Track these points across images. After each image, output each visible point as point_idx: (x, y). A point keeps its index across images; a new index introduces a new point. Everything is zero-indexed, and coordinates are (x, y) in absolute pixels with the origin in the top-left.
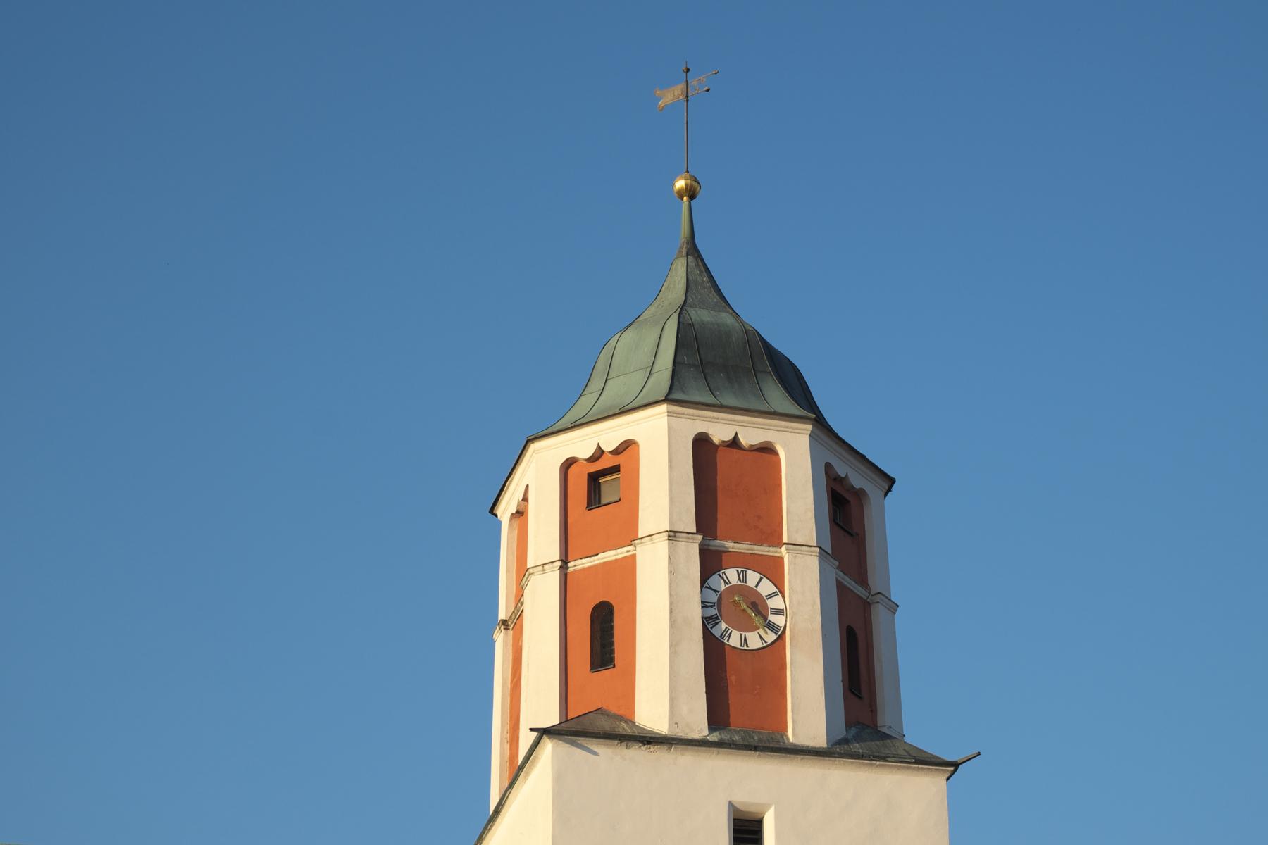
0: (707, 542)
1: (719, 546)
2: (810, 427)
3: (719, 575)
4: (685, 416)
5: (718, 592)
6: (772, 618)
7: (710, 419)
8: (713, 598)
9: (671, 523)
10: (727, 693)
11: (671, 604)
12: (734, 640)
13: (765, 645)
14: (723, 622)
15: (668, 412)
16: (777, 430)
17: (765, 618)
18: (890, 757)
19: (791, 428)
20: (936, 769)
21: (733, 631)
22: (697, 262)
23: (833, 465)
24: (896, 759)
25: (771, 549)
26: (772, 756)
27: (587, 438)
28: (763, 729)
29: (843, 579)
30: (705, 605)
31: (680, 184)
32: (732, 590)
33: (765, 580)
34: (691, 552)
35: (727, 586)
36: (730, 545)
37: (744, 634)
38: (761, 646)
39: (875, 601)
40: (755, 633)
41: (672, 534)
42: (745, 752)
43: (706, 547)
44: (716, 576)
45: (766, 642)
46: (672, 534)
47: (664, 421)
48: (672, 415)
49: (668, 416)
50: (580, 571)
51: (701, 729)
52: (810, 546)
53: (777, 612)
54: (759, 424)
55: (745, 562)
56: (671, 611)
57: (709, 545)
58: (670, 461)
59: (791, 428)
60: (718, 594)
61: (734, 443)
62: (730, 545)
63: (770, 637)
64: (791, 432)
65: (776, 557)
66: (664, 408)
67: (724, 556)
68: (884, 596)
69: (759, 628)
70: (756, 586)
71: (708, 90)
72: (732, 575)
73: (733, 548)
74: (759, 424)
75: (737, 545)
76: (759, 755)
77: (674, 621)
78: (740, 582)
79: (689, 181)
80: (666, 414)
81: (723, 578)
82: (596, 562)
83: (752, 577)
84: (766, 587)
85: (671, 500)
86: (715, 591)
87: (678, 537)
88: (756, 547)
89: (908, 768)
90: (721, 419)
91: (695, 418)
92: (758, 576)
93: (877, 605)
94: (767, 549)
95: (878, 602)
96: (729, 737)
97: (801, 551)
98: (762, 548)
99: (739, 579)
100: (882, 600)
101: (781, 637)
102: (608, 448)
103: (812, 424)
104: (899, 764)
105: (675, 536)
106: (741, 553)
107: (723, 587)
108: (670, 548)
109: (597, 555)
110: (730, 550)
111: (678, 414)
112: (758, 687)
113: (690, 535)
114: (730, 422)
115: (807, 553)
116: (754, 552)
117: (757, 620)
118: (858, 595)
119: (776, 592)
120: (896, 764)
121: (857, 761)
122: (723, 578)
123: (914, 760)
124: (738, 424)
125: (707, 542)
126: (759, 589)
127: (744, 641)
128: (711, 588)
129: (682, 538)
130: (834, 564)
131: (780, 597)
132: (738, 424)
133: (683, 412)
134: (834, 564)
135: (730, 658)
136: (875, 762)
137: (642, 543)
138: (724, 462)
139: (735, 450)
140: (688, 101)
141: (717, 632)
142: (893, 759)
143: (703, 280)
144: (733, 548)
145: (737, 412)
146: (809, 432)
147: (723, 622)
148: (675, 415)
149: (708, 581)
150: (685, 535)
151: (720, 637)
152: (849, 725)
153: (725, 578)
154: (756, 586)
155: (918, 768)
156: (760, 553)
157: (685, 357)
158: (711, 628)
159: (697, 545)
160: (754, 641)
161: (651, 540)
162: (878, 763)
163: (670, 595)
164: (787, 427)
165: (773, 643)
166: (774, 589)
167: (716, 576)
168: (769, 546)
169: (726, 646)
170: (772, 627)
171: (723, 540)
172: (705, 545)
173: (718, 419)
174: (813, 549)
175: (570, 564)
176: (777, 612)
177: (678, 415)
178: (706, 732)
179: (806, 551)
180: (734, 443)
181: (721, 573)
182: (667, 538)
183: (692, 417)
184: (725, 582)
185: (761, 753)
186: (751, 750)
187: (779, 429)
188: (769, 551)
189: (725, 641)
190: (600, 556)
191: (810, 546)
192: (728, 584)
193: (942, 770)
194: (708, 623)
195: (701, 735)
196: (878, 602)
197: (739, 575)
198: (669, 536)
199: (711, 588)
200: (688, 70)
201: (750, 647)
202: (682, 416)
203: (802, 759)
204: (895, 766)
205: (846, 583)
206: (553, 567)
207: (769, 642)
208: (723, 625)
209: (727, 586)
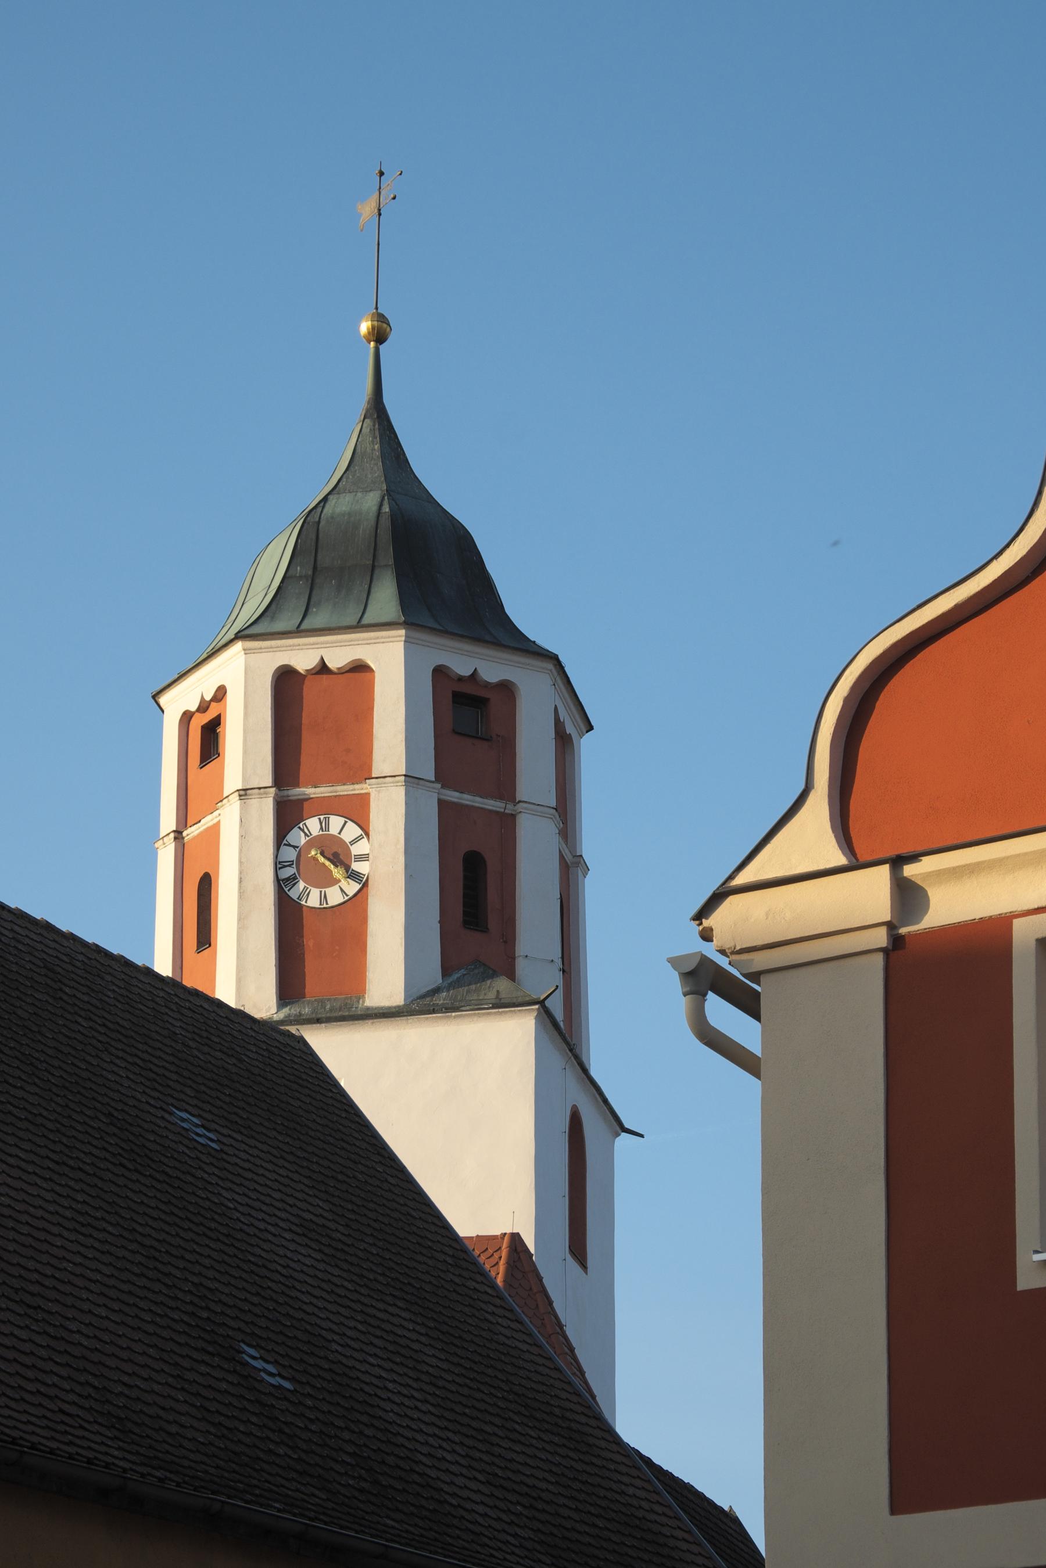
0: (285, 793)
1: (299, 795)
2: (402, 632)
3: (299, 828)
4: (264, 650)
5: (297, 847)
6: (356, 866)
7: (292, 648)
8: (289, 854)
9: (244, 779)
10: (302, 960)
11: (241, 873)
12: (313, 900)
13: (346, 898)
14: (301, 881)
15: (244, 650)
16: (368, 644)
17: (347, 868)
18: (462, 1006)
19: (382, 637)
20: (519, 1011)
21: (312, 888)
22: (374, 426)
23: (450, 666)
24: (471, 1007)
25: (356, 786)
26: (341, 1026)
27: (348, 644)
28: (341, 994)
29: (461, 799)
30: (279, 865)
31: (365, 327)
32: (313, 842)
33: (350, 823)
34: (265, 809)
35: (307, 838)
36: (311, 791)
37: (323, 890)
38: (342, 900)
39: (518, 811)
40: (337, 887)
41: (242, 793)
42: (309, 1026)
43: (285, 799)
44: (296, 829)
45: (347, 895)
46: (242, 793)
47: (242, 657)
48: (249, 652)
49: (245, 654)
50: (195, 838)
51: (269, 1007)
52: (394, 776)
53: (363, 858)
54: (345, 641)
55: (327, 807)
56: (241, 881)
57: (288, 796)
58: (246, 707)
59: (382, 637)
60: (298, 850)
61: (322, 668)
62: (311, 791)
63: (352, 888)
64: (383, 643)
65: (361, 794)
66: (239, 646)
67: (306, 804)
68: (526, 802)
69: (339, 881)
70: (340, 833)
71: (394, 198)
72: (313, 825)
73: (314, 794)
74: (345, 641)
75: (318, 790)
76: (326, 1026)
77: (244, 892)
78: (323, 831)
79: (376, 323)
80: (243, 652)
81: (303, 831)
82: (202, 829)
83: (336, 823)
84: (352, 831)
85: (245, 752)
86: (295, 847)
87: (250, 795)
88: (339, 788)
89: (489, 1014)
90: (303, 645)
91: (275, 649)
92: (342, 820)
93: (520, 815)
94: (351, 787)
95: (520, 812)
96: (298, 1010)
97: (385, 783)
98: (345, 787)
99: (321, 828)
100: (526, 809)
101: (365, 885)
102: (333, 664)
103: (405, 628)
104: (477, 1012)
105: (246, 795)
106: (324, 797)
107: (303, 840)
108: (242, 808)
109: (200, 821)
110: (312, 796)
111: (255, 649)
112: (337, 948)
113: (262, 790)
114: (313, 646)
115: (392, 785)
116: (338, 794)
117: (337, 873)
118: (490, 811)
119: (362, 835)
120: (473, 1012)
121: (430, 1016)
122: (303, 831)
123: (491, 1005)
124: (322, 646)
125: (285, 793)
126: (343, 836)
127: (324, 898)
128: (289, 845)
129: (255, 794)
130: (434, 788)
131: (365, 839)
132: (322, 646)
133: (259, 647)
134: (434, 788)
135: (308, 920)
136: (450, 1014)
137: (223, 806)
138: (312, 693)
139: (324, 676)
140: (380, 215)
141: (294, 894)
142: (468, 1008)
143: (373, 449)
144: (314, 794)
145: (318, 633)
146: (403, 639)
147: (301, 881)
148: (253, 651)
149: (287, 838)
150: (257, 791)
151: (298, 899)
152: (446, 970)
153: (306, 830)
154: (340, 833)
155: (499, 1012)
156: (346, 793)
157: (299, 568)
158: (289, 890)
159: (272, 799)
160: (335, 897)
161: (229, 801)
162: (453, 1014)
163: (241, 863)
164: (378, 638)
165: (355, 895)
166: (359, 832)
167: (296, 829)
168: (353, 784)
169: (304, 908)
170: (354, 876)
171: (303, 787)
172: (284, 796)
173: (299, 645)
174: (397, 778)
175: (185, 834)
176: (363, 858)
177: (255, 651)
178: (274, 1010)
179: (391, 783)
180: (322, 668)
181: (301, 825)
182: (238, 798)
183: (271, 650)
184: (306, 835)
185: (326, 1025)
186: (314, 1023)
187: (369, 642)
188: (354, 790)
189: (303, 903)
190: (203, 821)
191: (394, 776)
192: (308, 836)
193: (526, 1010)
194: (282, 886)
195: (268, 1014)
196: (520, 812)
197: (321, 823)
198: (240, 796)
199: (289, 845)
200: (381, 174)
201: (331, 904)
202: (260, 651)
203: (373, 1023)
204: (475, 1014)
205: (467, 803)
206: (170, 840)
207: (351, 894)
208: (301, 885)
209: (307, 838)
